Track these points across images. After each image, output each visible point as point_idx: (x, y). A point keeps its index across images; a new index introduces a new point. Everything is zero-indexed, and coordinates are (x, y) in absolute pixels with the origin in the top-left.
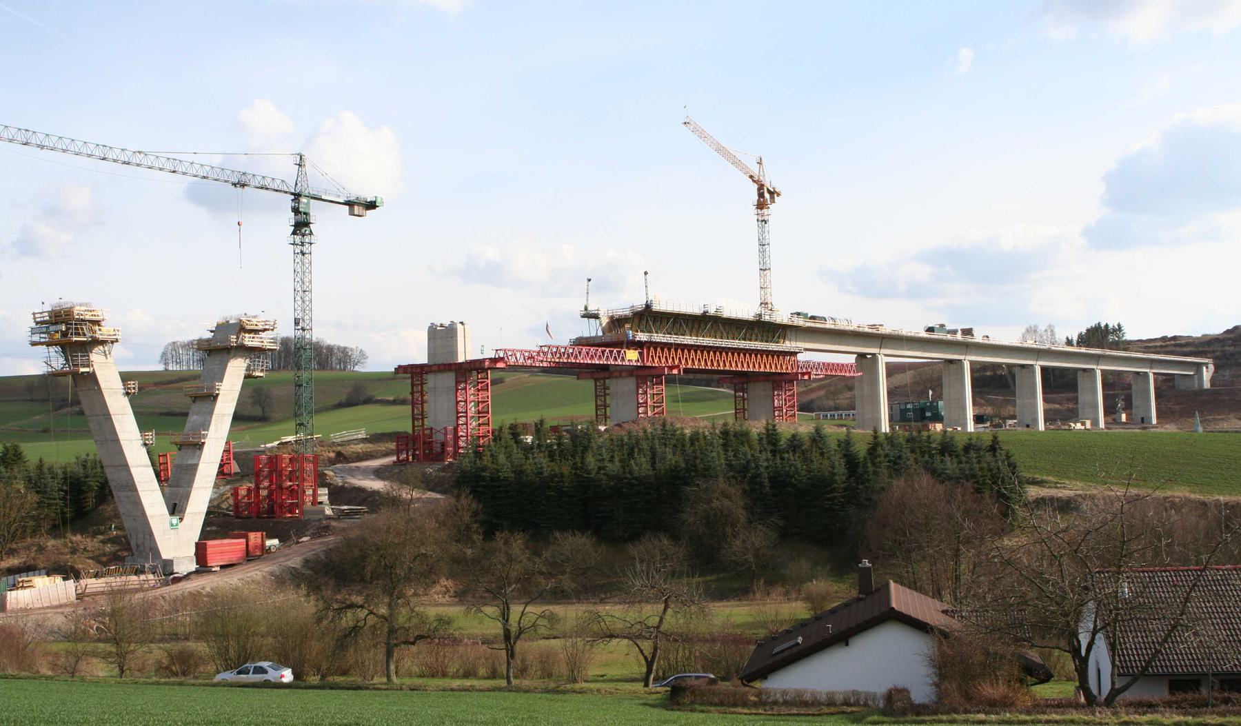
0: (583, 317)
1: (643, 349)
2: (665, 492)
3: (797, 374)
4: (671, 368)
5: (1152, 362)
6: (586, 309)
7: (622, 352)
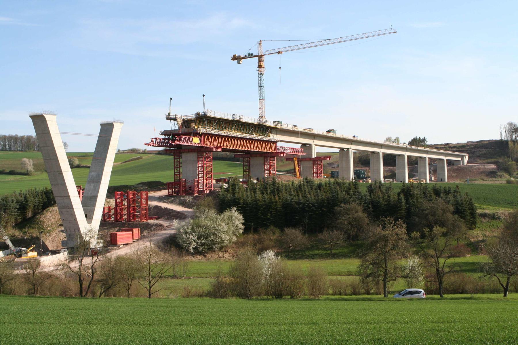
1: (201, 137)
2: (325, 210)
3: (278, 153)
4: (217, 148)
5: (446, 155)
6: (169, 115)
7: (191, 138)
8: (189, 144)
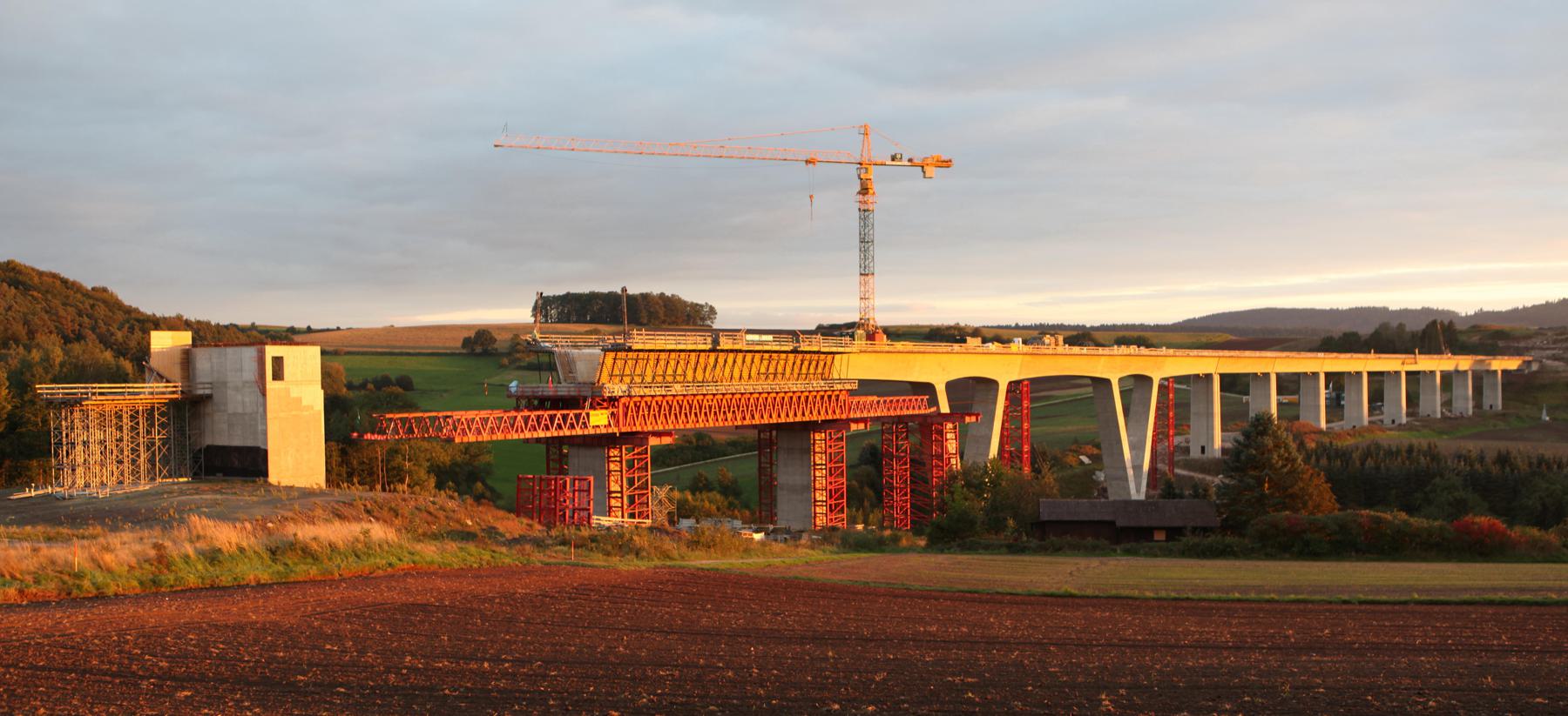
7: (584, 414)
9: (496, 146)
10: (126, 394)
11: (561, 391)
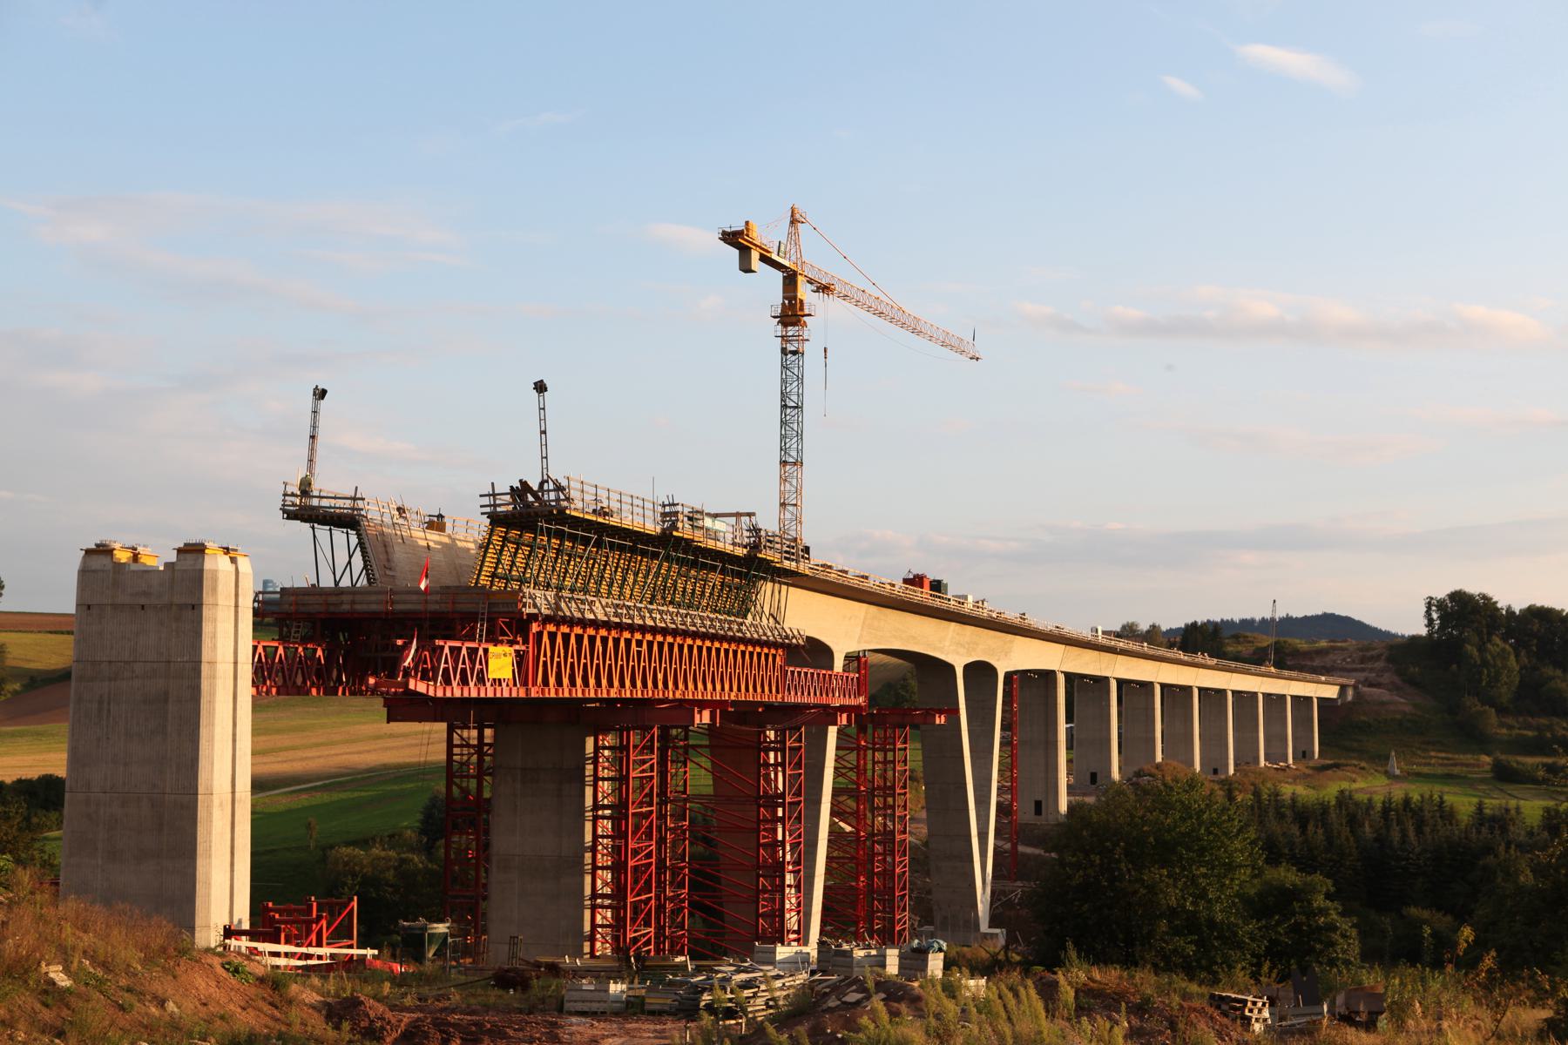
0: (291, 516)
6: (305, 488)
8: (473, 691)
9: (1274, 601)
10: (501, 606)
11: (405, 602)
